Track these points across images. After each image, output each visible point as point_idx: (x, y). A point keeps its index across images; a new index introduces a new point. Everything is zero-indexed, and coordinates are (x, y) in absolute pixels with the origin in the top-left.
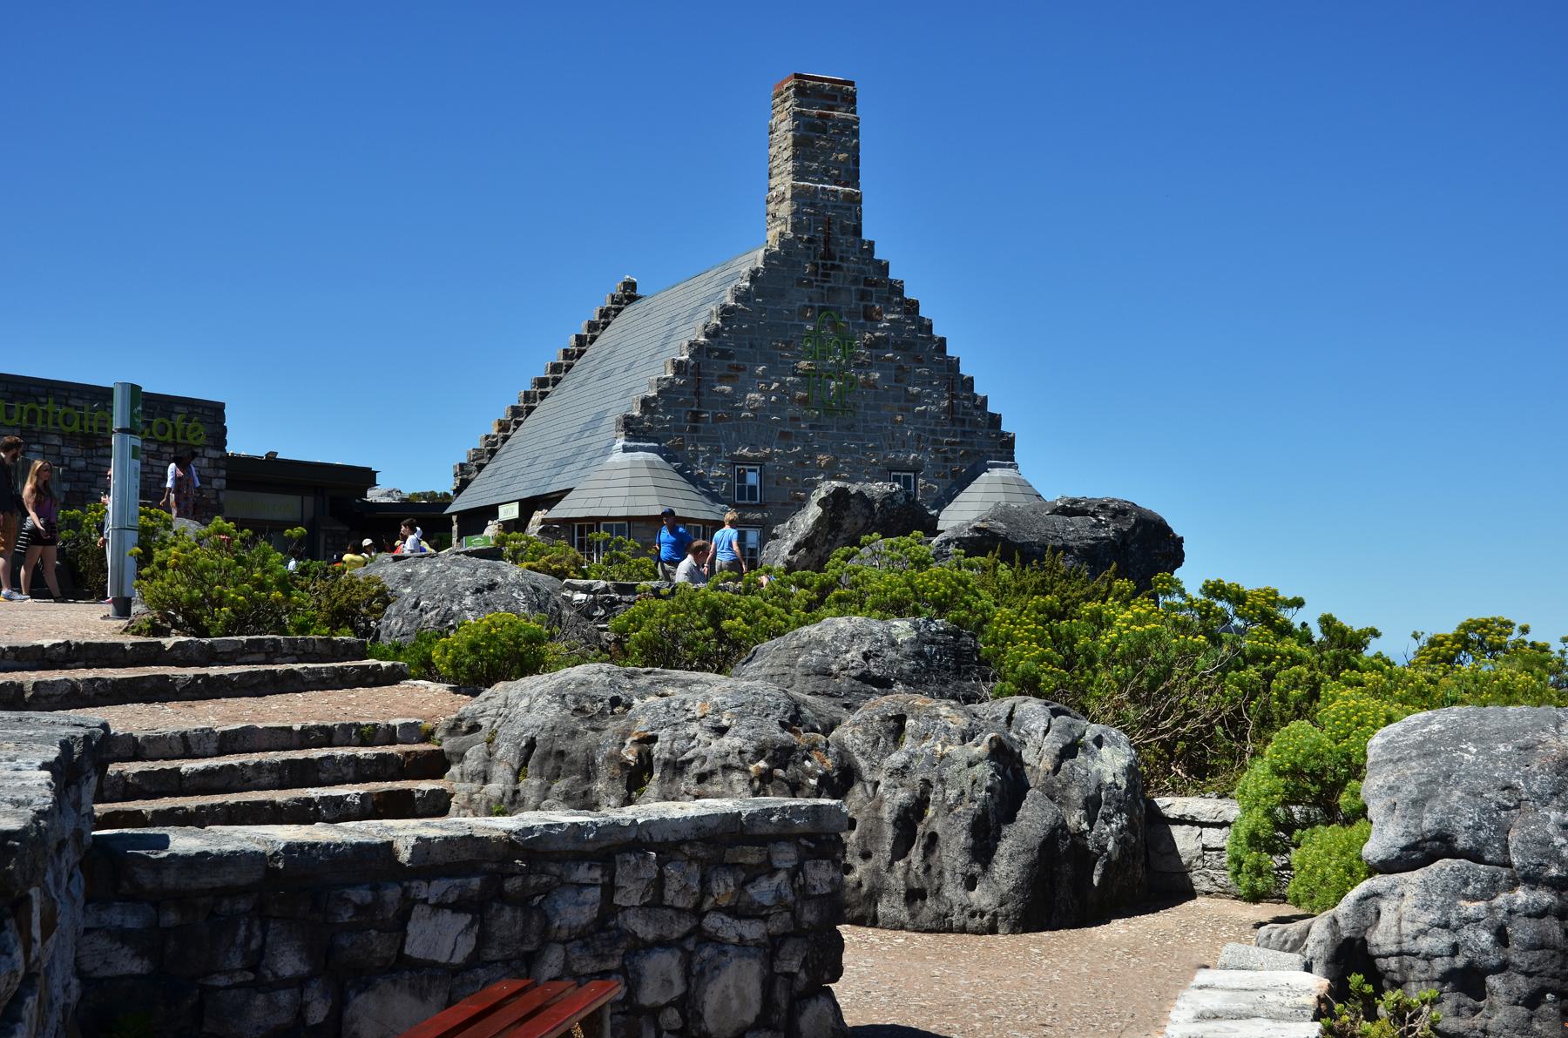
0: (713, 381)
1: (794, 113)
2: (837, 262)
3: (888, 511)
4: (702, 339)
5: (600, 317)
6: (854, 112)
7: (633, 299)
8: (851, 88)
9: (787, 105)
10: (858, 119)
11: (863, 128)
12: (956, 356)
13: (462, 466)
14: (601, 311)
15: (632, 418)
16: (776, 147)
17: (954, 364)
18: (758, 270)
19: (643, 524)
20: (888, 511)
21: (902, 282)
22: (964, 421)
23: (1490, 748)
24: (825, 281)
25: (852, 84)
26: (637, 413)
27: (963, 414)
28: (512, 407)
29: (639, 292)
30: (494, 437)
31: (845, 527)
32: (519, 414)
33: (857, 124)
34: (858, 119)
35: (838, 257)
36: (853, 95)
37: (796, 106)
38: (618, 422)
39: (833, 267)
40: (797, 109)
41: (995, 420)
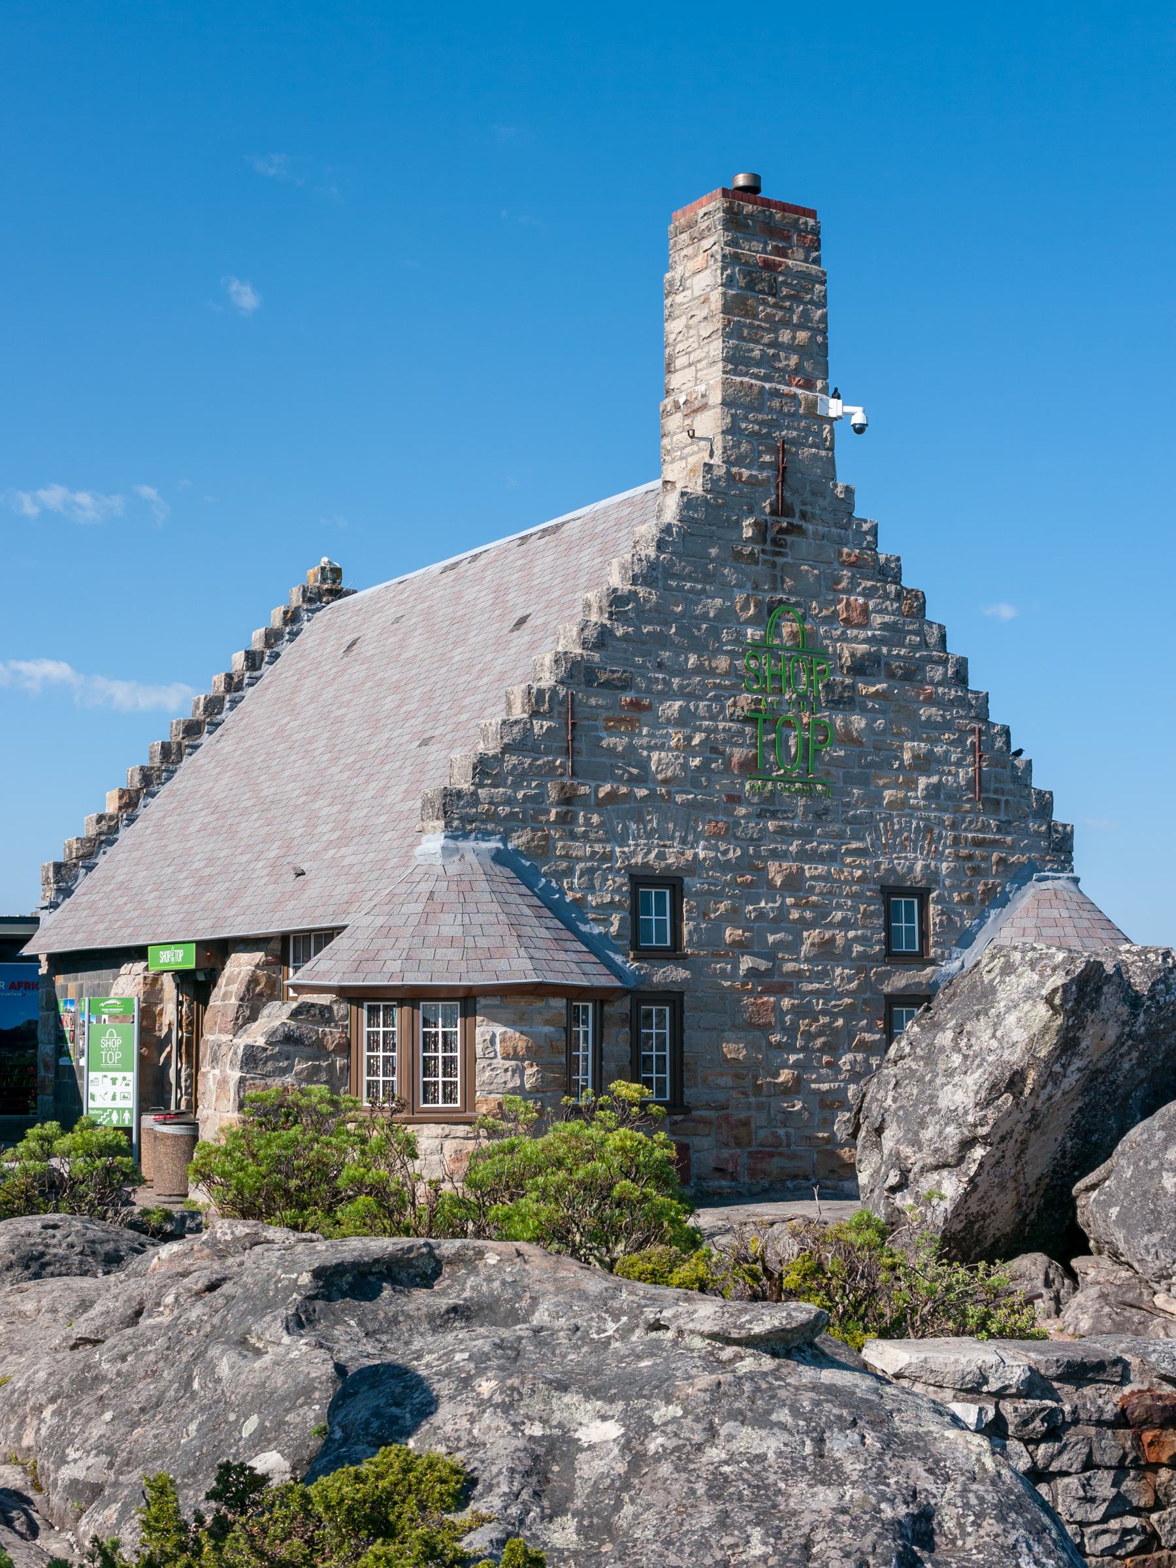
0: (596, 728)
1: (724, 256)
2: (796, 521)
3: (1160, 1008)
4: (579, 651)
5: (285, 624)
6: (816, 261)
7: (337, 594)
8: (811, 222)
9: (706, 244)
10: (825, 274)
11: (833, 289)
12: (985, 691)
13: (58, 867)
14: (285, 613)
15: (459, 794)
16: (684, 319)
17: (980, 707)
18: (668, 529)
19: (496, 1001)
20: (1160, 1008)
21: (898, 559)
22: (998, 802)
23: (140, 902)
24: (778, 554)
25: (812, 214)
26: (466, 786)
27: (996, 792)
28: (142, 769)
29: (345, 585)
30: (111, 818)
31: (1084, 1045)
32: (150, 780)
33: (823, 283)
34: (825, 274)
35: (797, 511)
36: (816, 232)
37: (726, 244)
38: (427, 803)
39: (791, 529)
40: (728, 250)
41: (1045, 804)
